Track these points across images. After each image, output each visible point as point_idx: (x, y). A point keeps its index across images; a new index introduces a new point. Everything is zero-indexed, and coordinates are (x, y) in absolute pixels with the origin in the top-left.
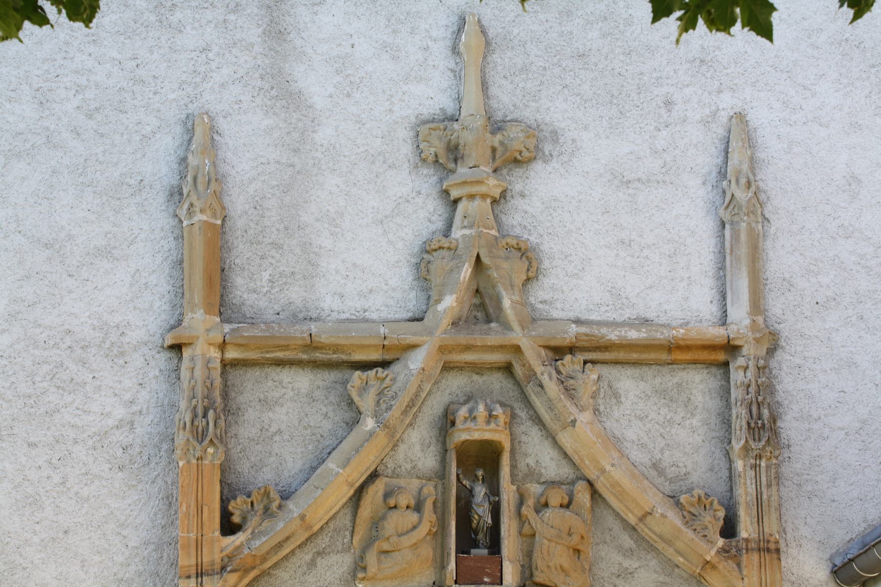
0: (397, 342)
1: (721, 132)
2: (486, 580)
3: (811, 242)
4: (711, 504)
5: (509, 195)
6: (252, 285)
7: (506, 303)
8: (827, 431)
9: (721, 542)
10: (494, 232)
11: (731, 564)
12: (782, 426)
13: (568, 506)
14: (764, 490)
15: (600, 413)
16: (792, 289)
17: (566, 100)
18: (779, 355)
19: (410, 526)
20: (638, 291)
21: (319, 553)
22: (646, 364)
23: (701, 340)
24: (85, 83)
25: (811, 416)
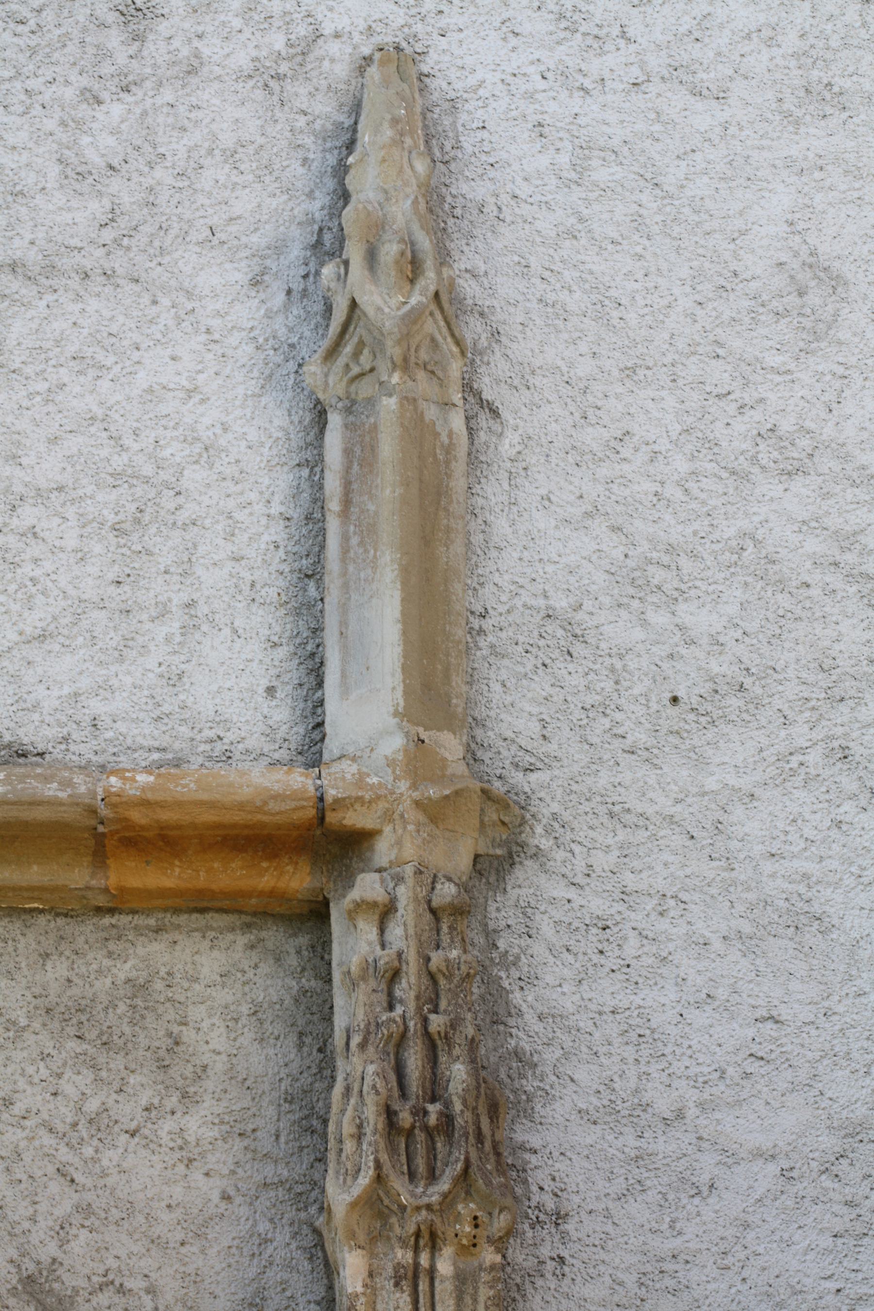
1: (326, 109)
3: (650, 487)
8: (707, 1165)
12: (535, 1141)
16: (578, 649)
18: (525, 881)
23: (212, 805)
25: (646, 1107)
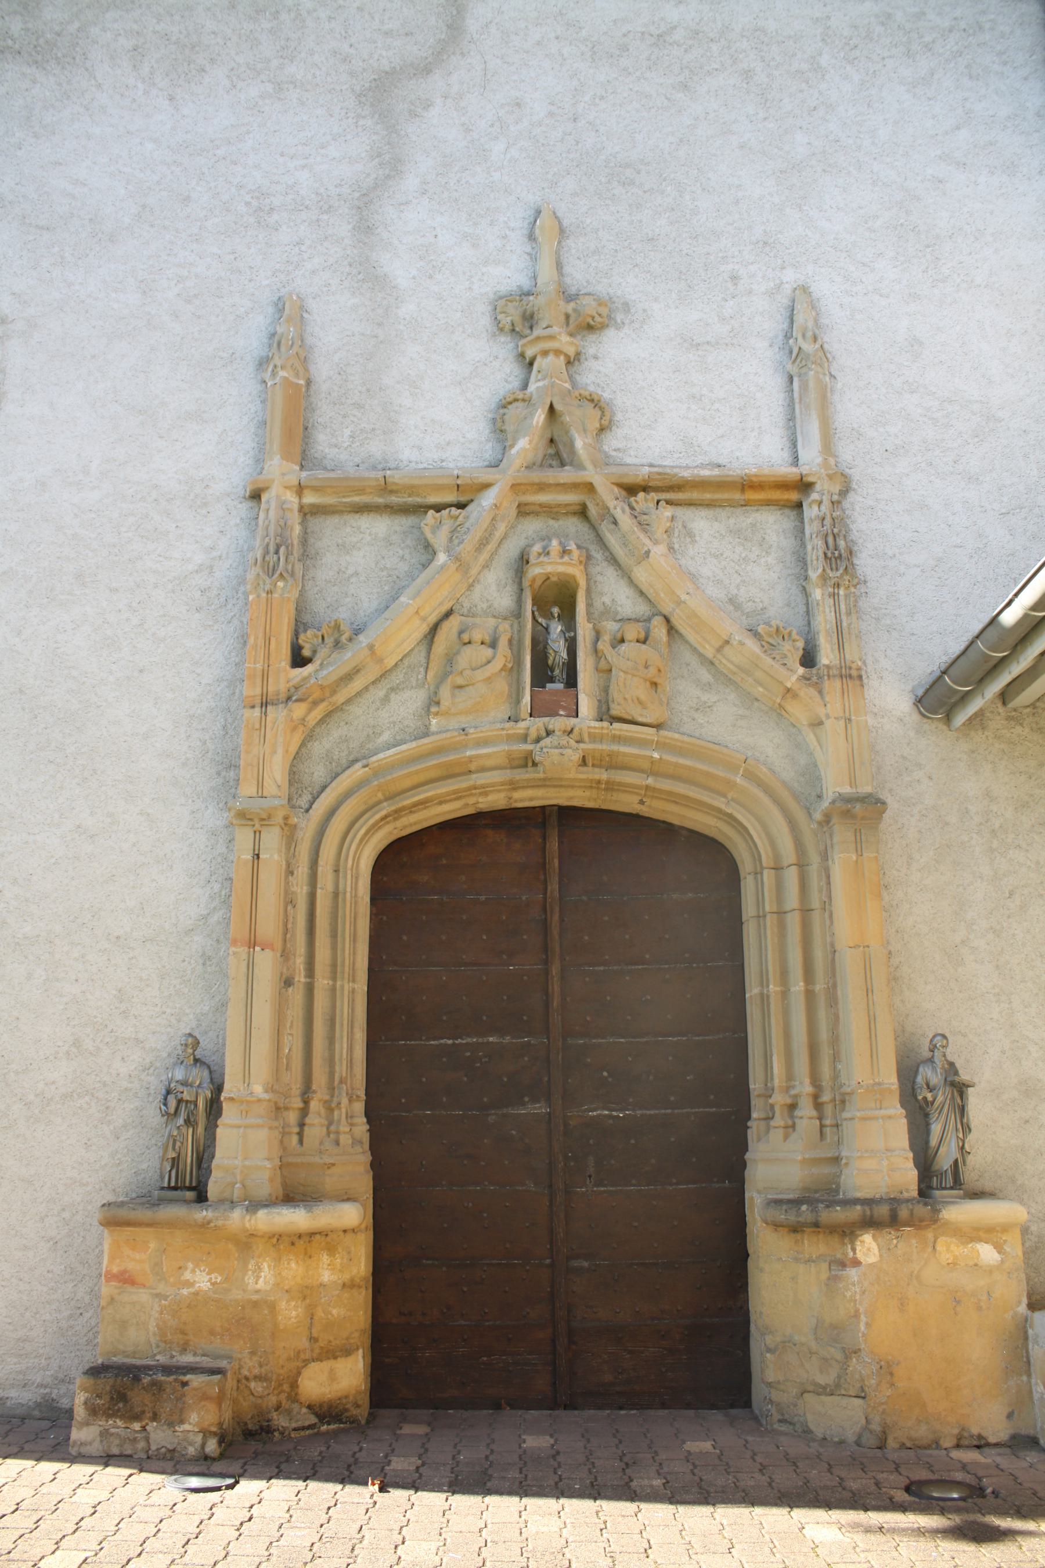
0: (470, 482)
1: (786, 302)
2: (561, 713)
4: (790, 634)
5: (582, 358)
6: (334, 440)
7: (579, 444)
9: (801, 670)
10: (567, 385)
11: (812, 692)
13: (644, 642)
14: (844, 617)
15: (675, 551)
17: (636, 277)
18: (852, 497)
19: (484, 660)
20: (710, 439)
21: (392, 689)
22: (720, 506)
23: (773, 476)
24: (186, 274)
